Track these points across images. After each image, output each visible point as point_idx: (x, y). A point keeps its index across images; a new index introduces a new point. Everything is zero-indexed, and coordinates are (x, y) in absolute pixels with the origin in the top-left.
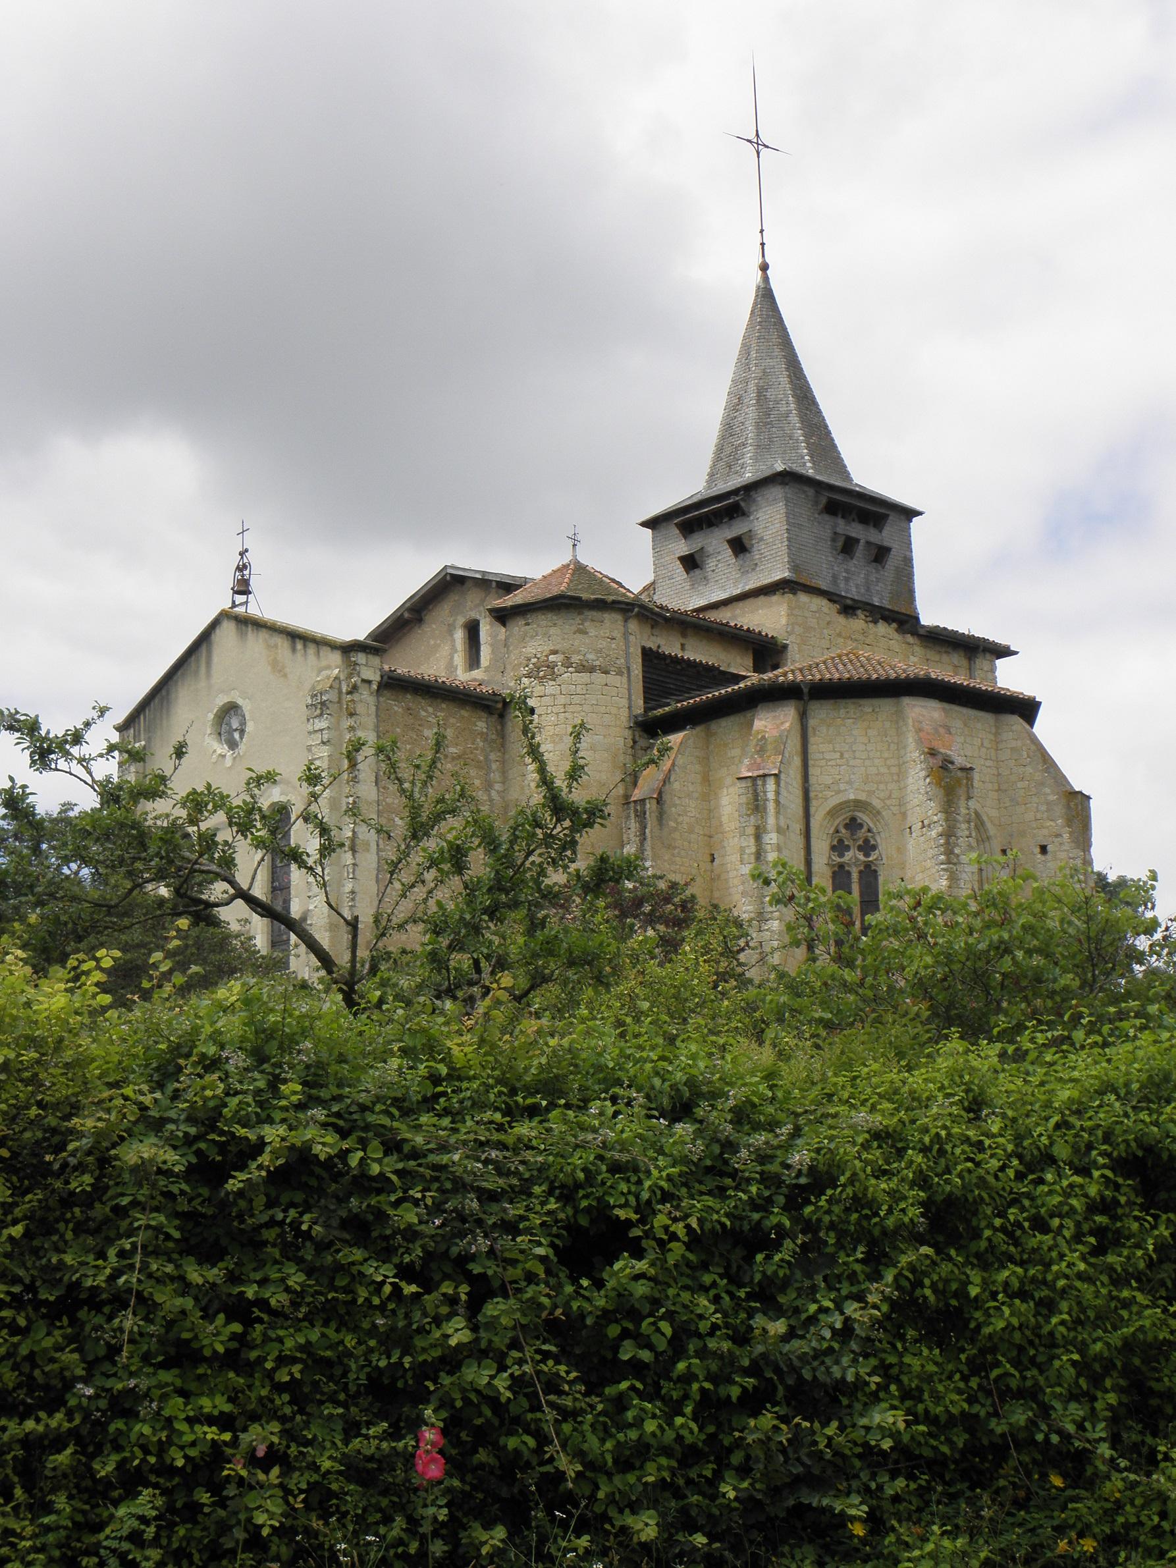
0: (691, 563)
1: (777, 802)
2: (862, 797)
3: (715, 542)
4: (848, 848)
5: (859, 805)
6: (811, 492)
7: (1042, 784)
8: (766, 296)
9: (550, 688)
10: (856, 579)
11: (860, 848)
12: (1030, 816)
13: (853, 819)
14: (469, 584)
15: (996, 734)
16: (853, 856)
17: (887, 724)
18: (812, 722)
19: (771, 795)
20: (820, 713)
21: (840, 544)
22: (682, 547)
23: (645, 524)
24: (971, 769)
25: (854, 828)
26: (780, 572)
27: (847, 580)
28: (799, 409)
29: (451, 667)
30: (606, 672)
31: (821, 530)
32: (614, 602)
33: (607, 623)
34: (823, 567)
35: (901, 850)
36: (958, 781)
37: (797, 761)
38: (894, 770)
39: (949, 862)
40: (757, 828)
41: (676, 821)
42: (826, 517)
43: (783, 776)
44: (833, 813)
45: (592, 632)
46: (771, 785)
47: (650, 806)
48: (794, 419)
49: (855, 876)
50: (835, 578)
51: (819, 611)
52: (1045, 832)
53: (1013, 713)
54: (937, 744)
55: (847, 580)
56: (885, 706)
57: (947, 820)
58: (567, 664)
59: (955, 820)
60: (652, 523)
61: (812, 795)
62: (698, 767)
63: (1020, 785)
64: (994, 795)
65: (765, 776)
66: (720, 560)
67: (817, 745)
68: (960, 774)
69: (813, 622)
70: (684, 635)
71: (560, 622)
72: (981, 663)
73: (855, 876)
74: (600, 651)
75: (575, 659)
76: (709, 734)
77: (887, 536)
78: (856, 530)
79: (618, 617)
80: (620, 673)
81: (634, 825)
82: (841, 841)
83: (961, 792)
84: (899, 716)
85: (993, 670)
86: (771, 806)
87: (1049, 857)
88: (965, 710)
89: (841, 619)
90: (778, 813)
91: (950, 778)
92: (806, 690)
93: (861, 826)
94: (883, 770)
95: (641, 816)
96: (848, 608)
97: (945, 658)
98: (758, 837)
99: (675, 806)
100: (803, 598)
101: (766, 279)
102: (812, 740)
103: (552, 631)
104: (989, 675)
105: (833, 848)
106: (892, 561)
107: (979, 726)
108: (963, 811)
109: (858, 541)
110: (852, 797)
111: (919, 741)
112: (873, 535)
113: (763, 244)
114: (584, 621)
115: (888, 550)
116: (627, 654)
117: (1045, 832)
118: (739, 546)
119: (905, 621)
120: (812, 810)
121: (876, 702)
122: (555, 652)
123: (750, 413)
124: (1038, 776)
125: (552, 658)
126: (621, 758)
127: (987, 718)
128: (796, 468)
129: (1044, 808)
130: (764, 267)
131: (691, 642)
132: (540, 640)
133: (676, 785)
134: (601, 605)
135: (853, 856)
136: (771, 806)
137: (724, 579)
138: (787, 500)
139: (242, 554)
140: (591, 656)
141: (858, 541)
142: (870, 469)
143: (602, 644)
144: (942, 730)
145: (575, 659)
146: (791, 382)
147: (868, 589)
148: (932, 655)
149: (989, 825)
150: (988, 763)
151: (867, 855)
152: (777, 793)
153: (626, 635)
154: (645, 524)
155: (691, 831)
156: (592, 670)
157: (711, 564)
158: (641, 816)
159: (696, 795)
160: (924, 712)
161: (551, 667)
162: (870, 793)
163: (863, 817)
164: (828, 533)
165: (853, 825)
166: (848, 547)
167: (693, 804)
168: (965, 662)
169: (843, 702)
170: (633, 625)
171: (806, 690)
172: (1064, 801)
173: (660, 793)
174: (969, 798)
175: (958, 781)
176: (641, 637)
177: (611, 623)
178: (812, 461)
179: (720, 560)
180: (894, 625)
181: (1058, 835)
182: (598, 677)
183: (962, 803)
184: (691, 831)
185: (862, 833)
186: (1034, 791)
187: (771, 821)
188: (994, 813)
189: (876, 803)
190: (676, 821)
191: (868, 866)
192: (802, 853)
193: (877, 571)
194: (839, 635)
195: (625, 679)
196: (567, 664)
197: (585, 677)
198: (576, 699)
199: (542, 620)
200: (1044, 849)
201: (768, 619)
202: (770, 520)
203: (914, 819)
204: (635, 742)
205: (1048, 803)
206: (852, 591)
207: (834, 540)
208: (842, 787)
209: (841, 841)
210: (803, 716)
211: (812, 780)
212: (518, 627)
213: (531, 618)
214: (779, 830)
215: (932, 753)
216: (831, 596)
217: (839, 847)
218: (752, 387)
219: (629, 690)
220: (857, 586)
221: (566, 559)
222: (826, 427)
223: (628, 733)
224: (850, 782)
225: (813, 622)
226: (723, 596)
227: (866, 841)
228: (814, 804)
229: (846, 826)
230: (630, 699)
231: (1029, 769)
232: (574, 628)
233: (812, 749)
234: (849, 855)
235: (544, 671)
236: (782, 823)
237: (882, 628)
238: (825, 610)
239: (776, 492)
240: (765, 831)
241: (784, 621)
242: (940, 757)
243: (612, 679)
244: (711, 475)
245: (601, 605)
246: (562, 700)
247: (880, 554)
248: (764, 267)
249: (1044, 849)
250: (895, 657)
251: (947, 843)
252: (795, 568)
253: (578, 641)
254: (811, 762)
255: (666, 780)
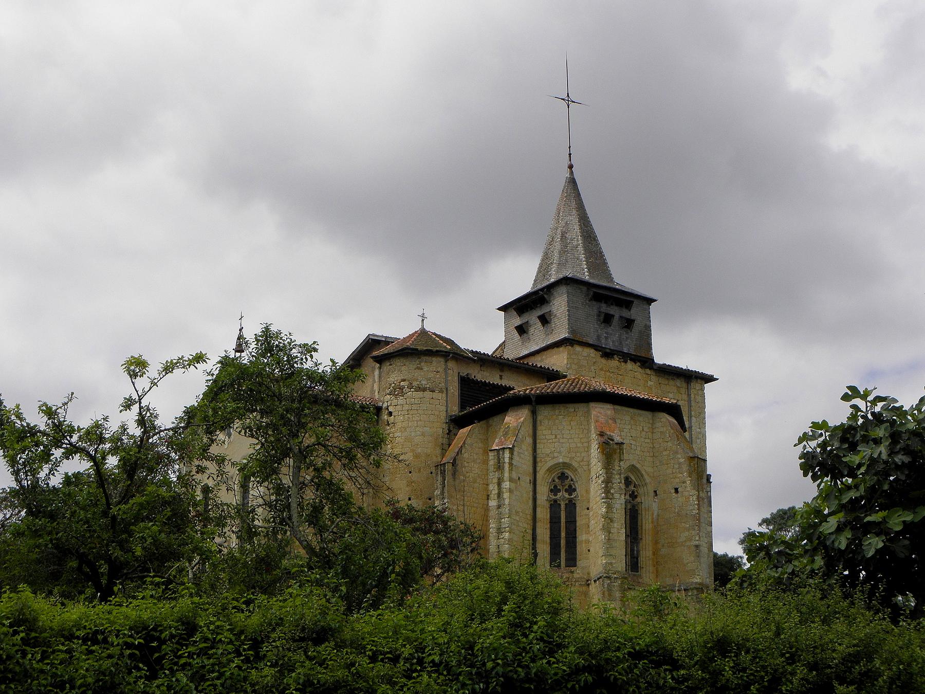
0: (522, 330)
1: (511, 464)
2: (567, 460)
3: (532, 317)
4: (559, 491)
5: (566, 465)
6: (584, 289)
7: (677, 453)
8: (572, 182)
9: (401, 400)
10: (613, 338)
11: (566, 490)
12: (669, 471)
13: (563, 474)
14: (382, 344)
15: (653, 424)
16: (563, 495)
17: (582, 418)
18: (539, 418)
19: (507, 460)
20: (544, 412)
21: (602, 318)
22: (518, 321)
23: (500, 309)
24: (622, 443)
25: (563, 479)
26: (564, 334)
27: (606, 338)
28: (584, 243)
29: (373, 391)
30: (433, 391)
31: (589, 312)
32: (437, 351)
33: (434, 363)
34: (592, 331)
35: (588, 491)
36: (615, 450)
37: (529, 440)
38: (586, 445)
39: (607, 498)
40: (499, 479)
41: (464, 476)
42: (594, 303)
43: (516, 449)
44: (550, 470)
45: (426, 369)
46: (507, 454)
47: (449, 467)
48: (581, 249)
49: (563, 507)
50: (599, 337)
51: (588, 356)
52: (677, 480)
53: (663, 411)
54: (604, 429)
55: (606, 338)
56: (581, 408)
57: (606, 473)
58: (410, 387)
59: (612, 473)
60: (504, 308)
61: (538, 460)
62: (481, 445)
63: (665, 453)
64: (651, 459)
65: (504, 448)
66: (536, 328)
67: (542, 431)
68: (615, 446)
69: (584, 363)
70: (502, 370)
71: (407, 363)
72: (695, 385)
73: (563, 507)
74: (430, 379)
75: (415, 384)
76: (488, 426)
77: (634, 312)
78: (614, 311)
79: (442, 360)
80: (441, 391)
81: (440, 478)
82: (555, 486)
83: (616, 457)
84: (588, 413)
85: (703, 389)
86: (507, 466)
87: (679, 495)
88: (631, 410)
89: (603, 361)
90: (511, 470)
91: (611, 450)
92: (533, 399)
93: (567, 477)
94: (579, 445)
95: (443, 473)
96: (608, 354)
97: (671, 382)
98: (499, 484)
99: (465, 467)
100: (578, 348)
101: (572, 173)
102: (539, 428)
103: (403, 368)
104: (700, 392)
105: (551, 491)
106: (637, 327)
107: (641, 419)
108: (617, 468)
109: (613, 316)
110: (561, 460)
111: (596, 427)
112: (625, 313)
113: (570, 154)
114: (420, 362)
115: (634, 321)
116: (446, 381)
117: (677, 480)
118: (545, 320)
119: (646, 362)
120: (538, 469)
121: (576, 405)
122: (404, 380)
123: (557, 246)
124: (674, 448)
125: (402, 384)
126: (440, 440)
127: (648, 414)
128: (579, 276)
129: (676, 466)
130: (571, 167)
131: (506, 375)
132: (398, 373)
133: (466, 455)
134: (429, 353)
135: (563, 495)
136: (507, 466)
137: (539, 338)
138: (568, 293)
139: (240, 330)
140: (424, 382)
141: (613, 316)
142: (624, 276)
143: (431, 375)
144: (610, 422)
145: (415, 384)
146: (581, 228)
147: (621, 343)
148: (662, 380)
149: (646, 477)
150: (647, 441)
151: (570, 494)
152: (511, 459)
153: (446, 369)
154: (500, 309)
155: (475, 482)
156: (424, 390)
157: (532, 330)
158: (443, 473)
159: (478, 461)
160: (602, 411)
161: (401, 388)
162: (572, 458)
163: (568, 472)
164: (595, 311)
165: (563, 477)
166: (607, 319)
167: (476, 466)
168: (684, 385)
169: (557, 406)
170: (451, 364)
171: (533, 399)
172: (687, 462)
173: (455, 460)
174: (620, 460)
175: (615, 450)
176: (454, 371)
177: (437, 364)
178: (589, 271)
179: (536, 328)
180: (638, 364)
181: (684, 482)
182: (428, 394)
183: (616, 463)
184: (475, 482)
185: (567, 482)
186: (672, 456)
187: (506, 475)
188: (650, 470)
189: (575, 464)
190: (464, 476)
191: (570, 501)
192: (531, 493)
193: (627, 333)
194: (602, 369)
195: (444, 395)
196: (410, 387)
197: (420, 394)
198: (414, 407)
199: (398, 362)
200: (676, 490)
201: (557, 361)
202: (560, 305)
203: (593, 474)
204: (450, 431)
205: (679, 464)
206: (610, 345)
207: (599, 316)
208: (556, 455)
209: (555, 486)
210: (534, 413)
211: (538, 451)
212: (386, 367)
213: (393, 361)
214: (511, 480)
215: (602, 434)
216: (596, 348)
217: (555, 490)
218: (559, 231)
219: (447, 401)
220: (613, 342)
221: (417, 327)
222: (601, 253)
223: (445, 426)
224: (560, 452)
225: (584, 363)
226: (536, 348)
227: (570, 486)
228: (539, 465)
229: (559, 478)
230: (447, 406)
231: (670, 444)
232: (415, 367)
233: (539, 433)
234: (559, 494)
235: (397, 391)
236: (514, 475)
237: (630, 365)
238: (592, 355)
239: (563, 290)
240: (503, 481)
241: (565, 362)
242: (606, 437)
243: (436, 395)
244: (535, 281)
245: (429, 353)
246: (406, 407)
247: (628, 324)
248: (571, 167)
249: (676, 490)
250: (632, 382)
251: (606, 487)
252: (572, 331)
253: (417, 374)
254: (538, 441)
255: (459, 452)
